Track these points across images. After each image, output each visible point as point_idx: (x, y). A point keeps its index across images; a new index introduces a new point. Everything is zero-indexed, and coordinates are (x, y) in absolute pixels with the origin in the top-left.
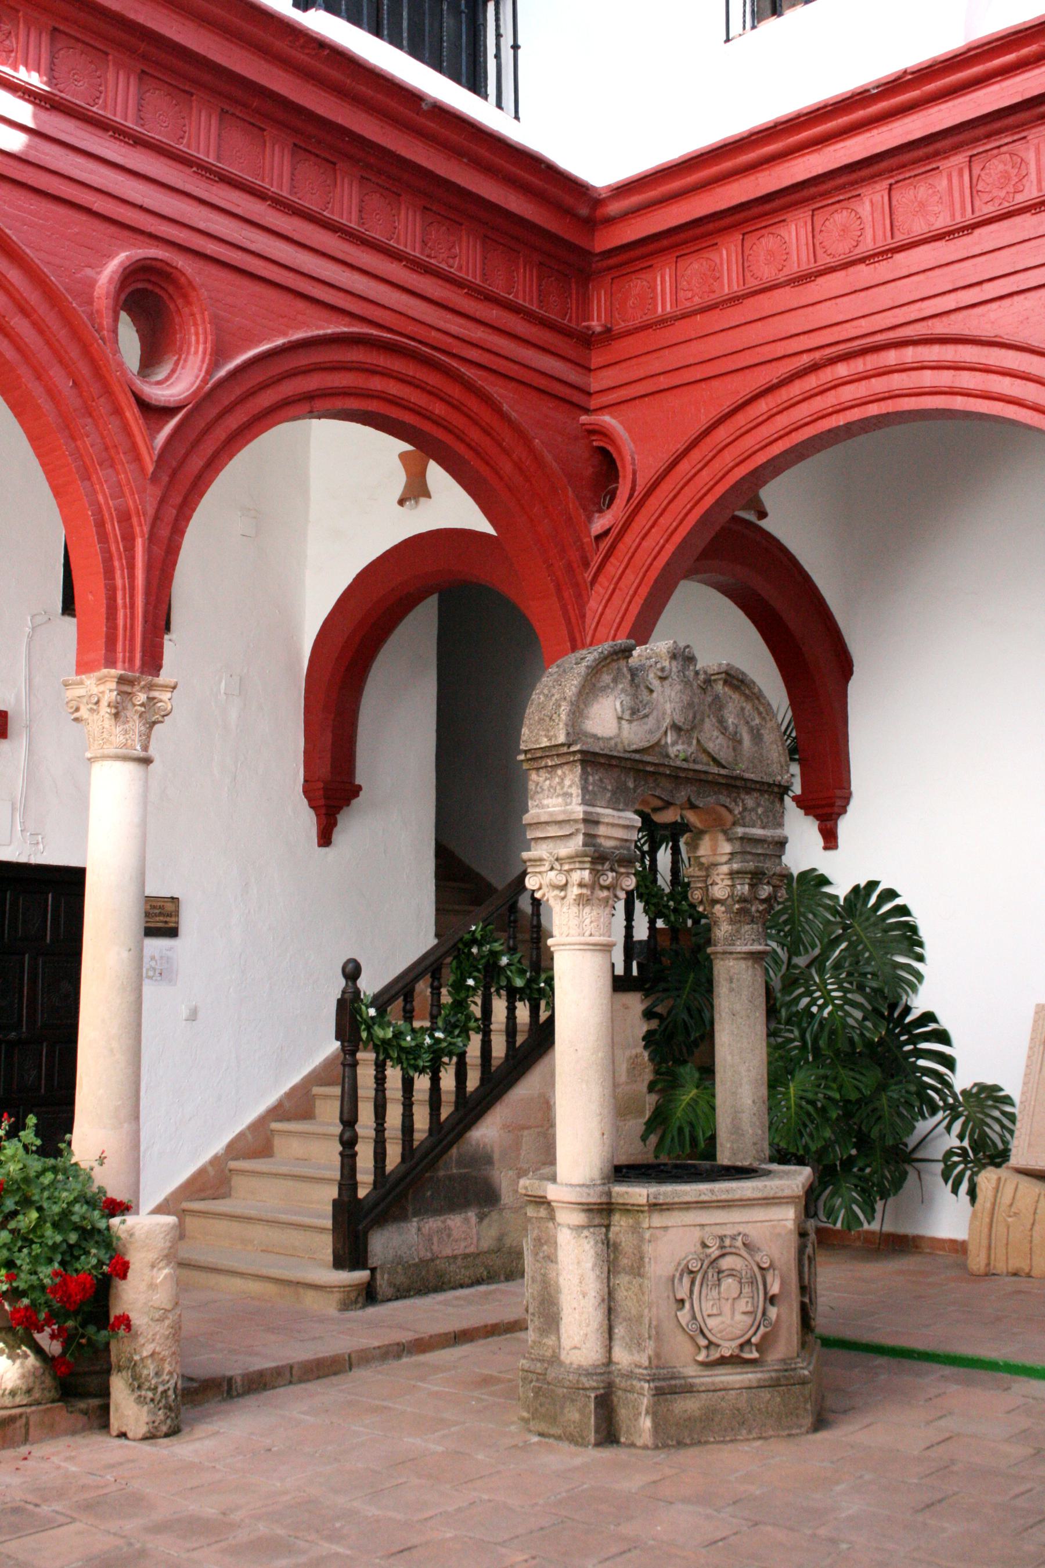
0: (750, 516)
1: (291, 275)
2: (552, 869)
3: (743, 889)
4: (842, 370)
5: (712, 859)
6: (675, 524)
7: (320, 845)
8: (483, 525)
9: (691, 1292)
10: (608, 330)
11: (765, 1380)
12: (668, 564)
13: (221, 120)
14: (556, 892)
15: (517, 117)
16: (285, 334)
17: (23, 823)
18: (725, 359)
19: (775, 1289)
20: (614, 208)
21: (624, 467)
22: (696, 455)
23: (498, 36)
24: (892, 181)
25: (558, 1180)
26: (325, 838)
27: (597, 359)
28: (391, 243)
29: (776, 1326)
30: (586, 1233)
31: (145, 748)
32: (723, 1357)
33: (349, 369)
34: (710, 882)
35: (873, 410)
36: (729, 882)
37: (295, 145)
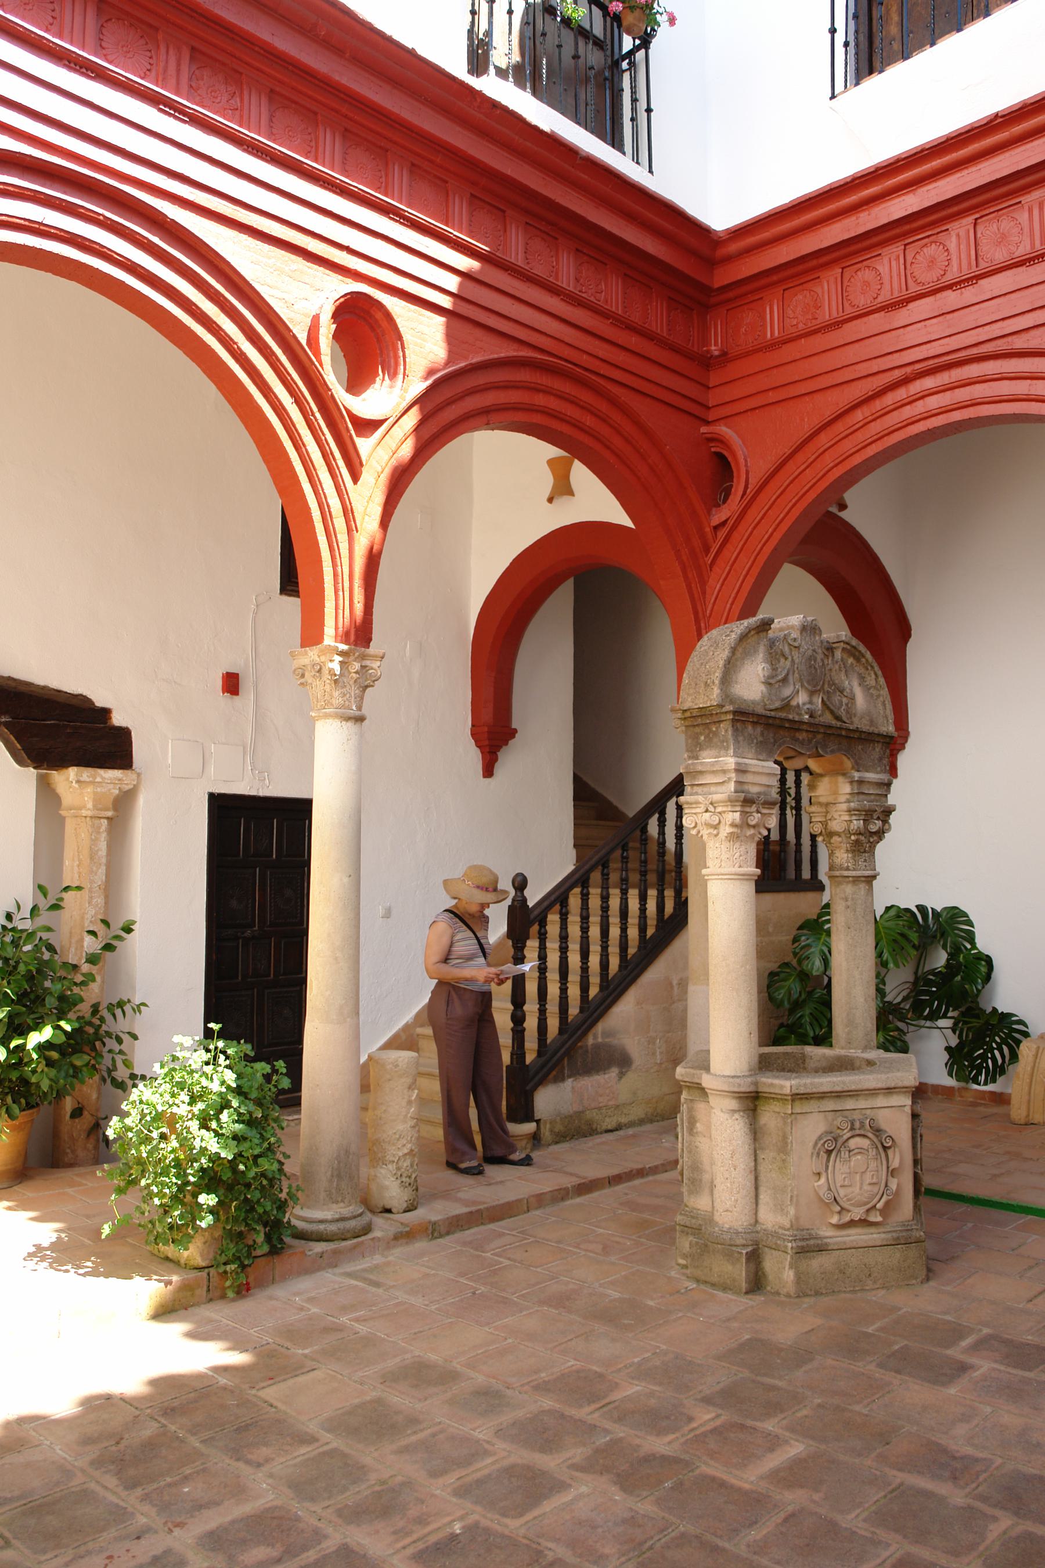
0: (834, 509)
1: (471, 307)
2: (707, 811)
3: (857, 824)
4: (929, 383)
5: (830, 799)
6: (782, 516)
7: (485, 776)
8: (624, 520)
9: (827, 1167)
10: (724, 354)
11: (887, 1240)
12: (775, 549)
13: (411, 172)
14: (711, 830)
15: (651, 171)
16: (466, 358)
17: (253, 764)
18: (826, 376)
19: (895, 1163)
20: (733, 248)
21: (738, 470)
22: (800, 457)
23: (634, 100)
24: (977, 216)
25: (712, 1071)
26: (488, 771)
27: (714, 379)
28: (551, 279)
29: (898, 1193)
30: (736, 1116)
31: (359, 708)
32: (852, 1221)
33: (517, 388)
34: (829, 817)
35: (957, 416)
36: (847, 818)
37: (472, 195)
